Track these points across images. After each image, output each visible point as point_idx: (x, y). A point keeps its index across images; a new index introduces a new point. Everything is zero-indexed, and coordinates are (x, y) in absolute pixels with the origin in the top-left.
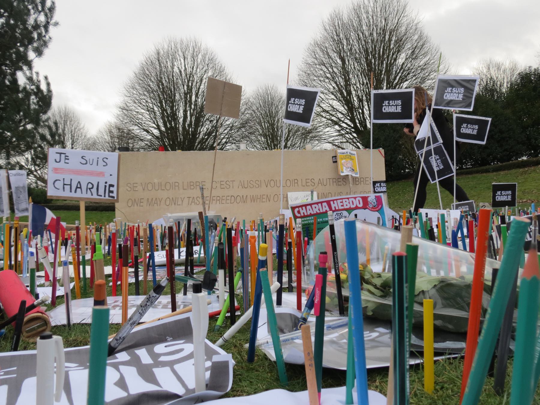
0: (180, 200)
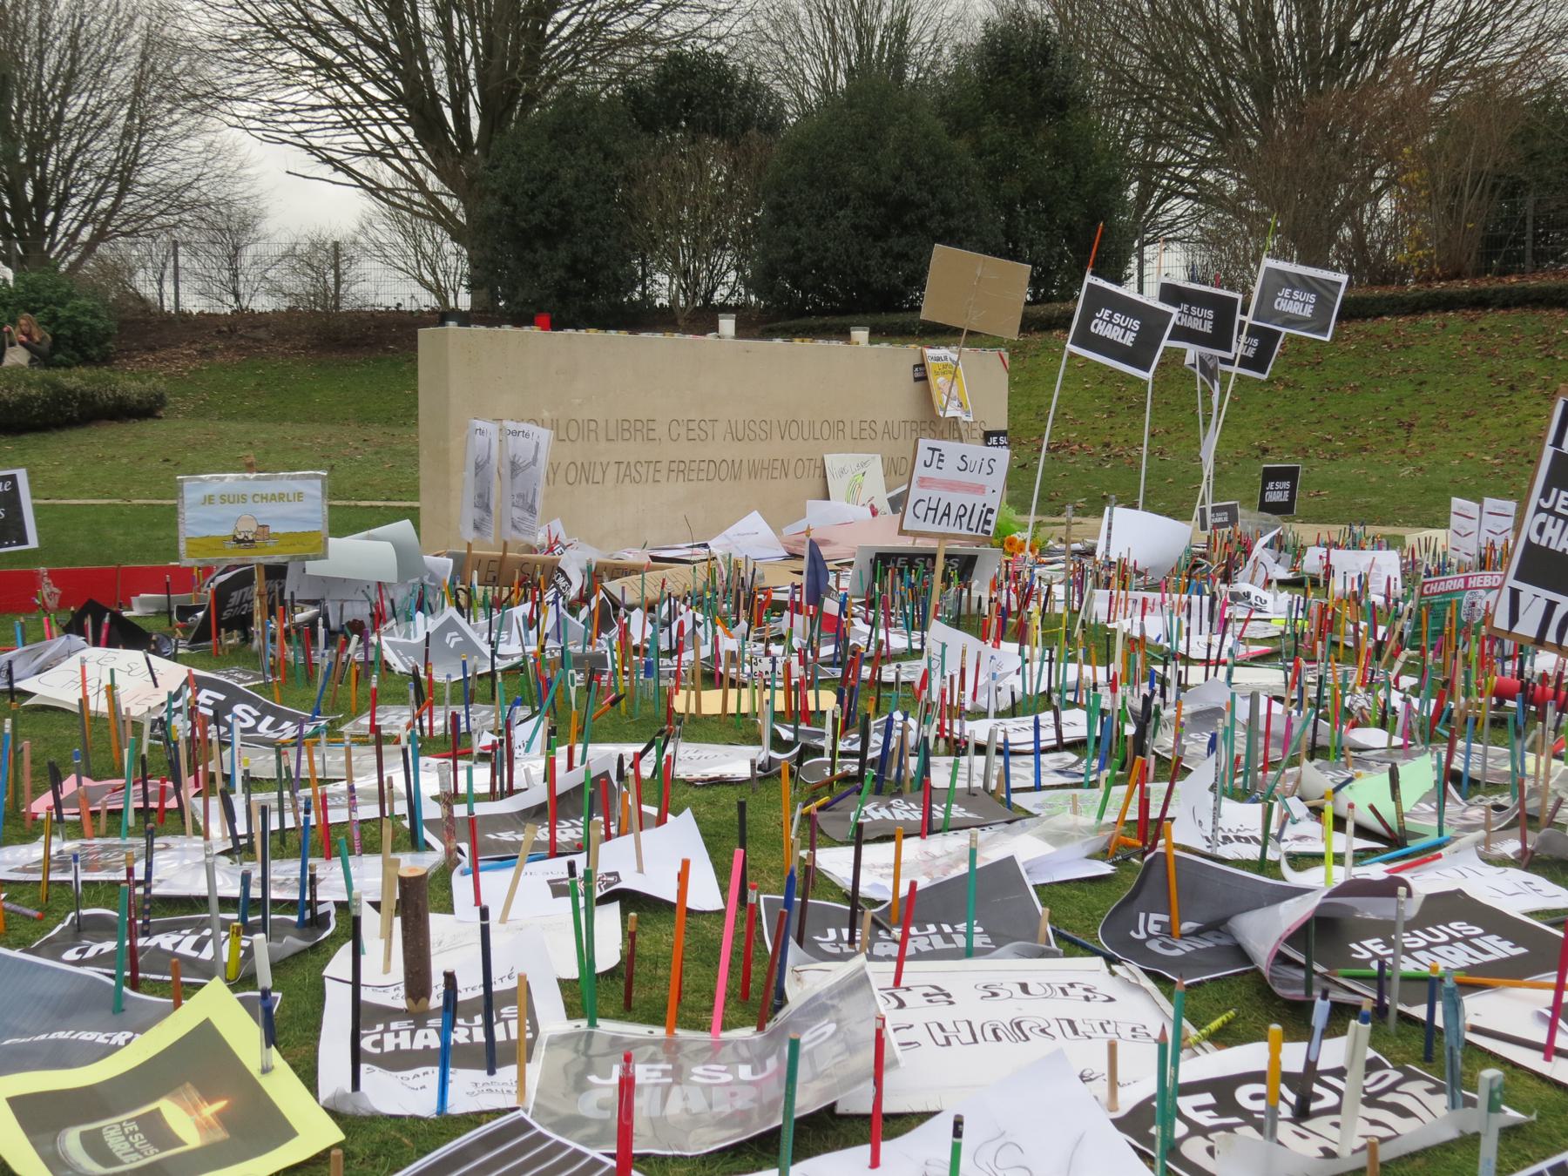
0: (598, 467)
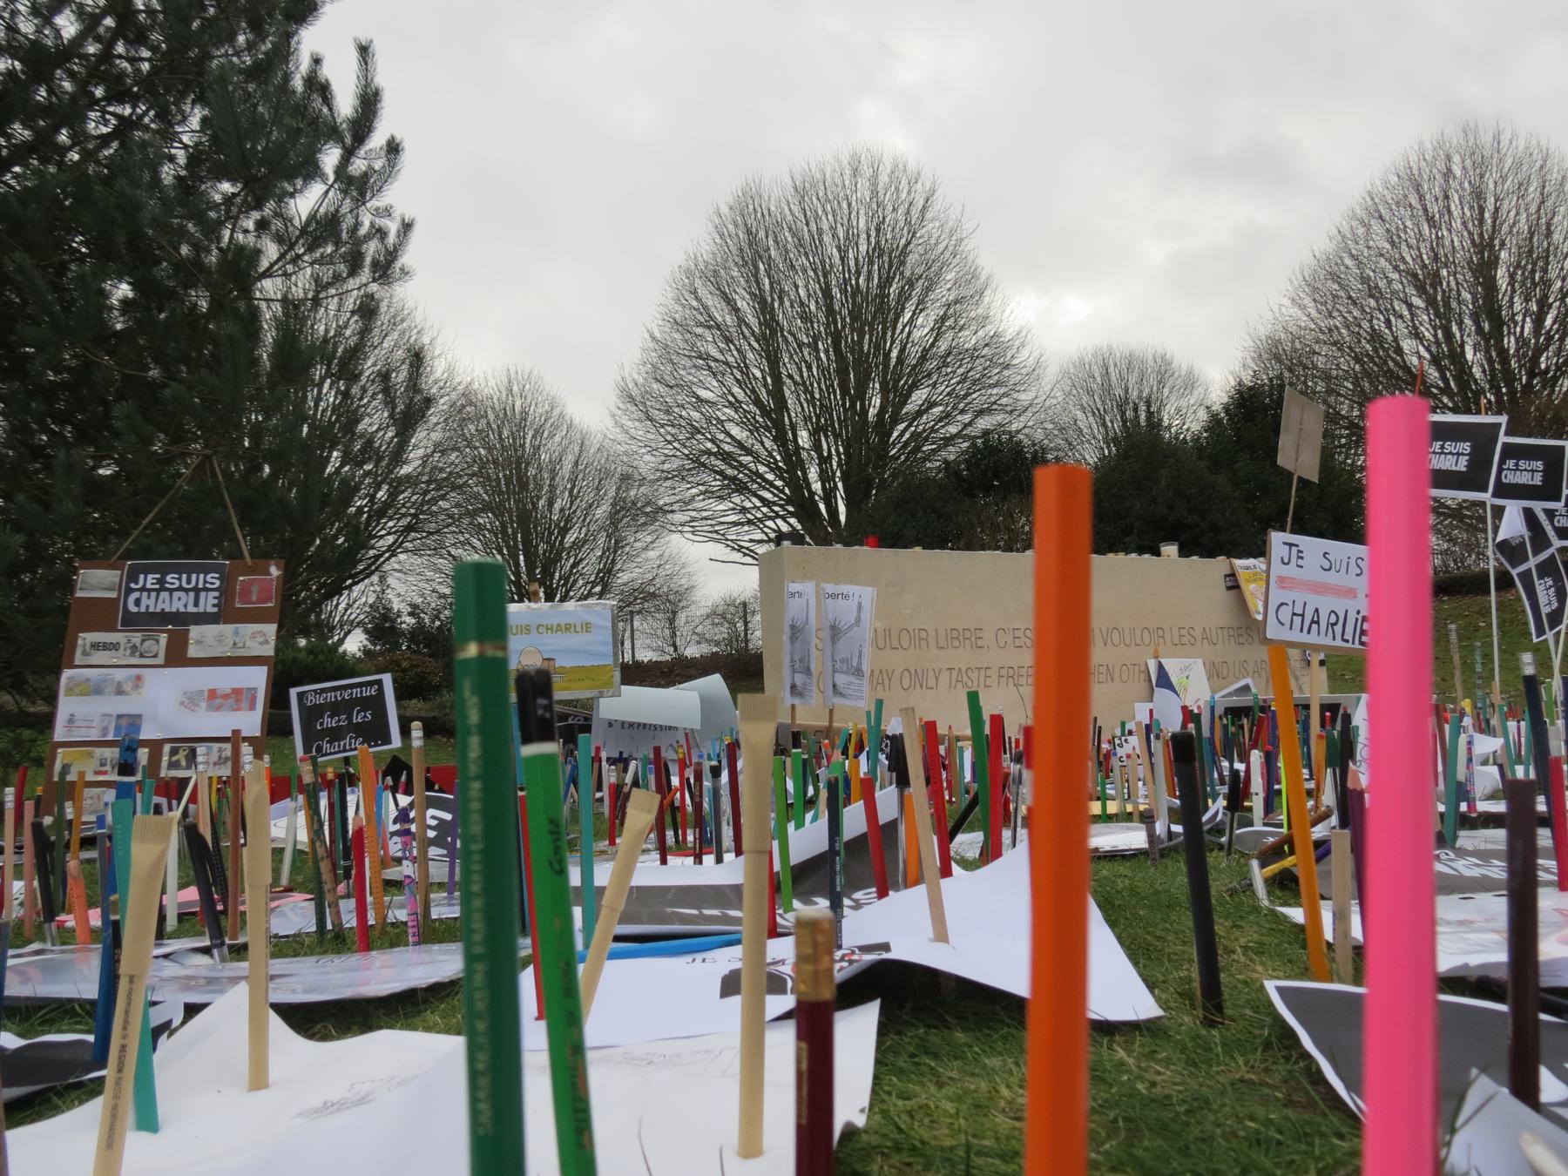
0: (931, 674)
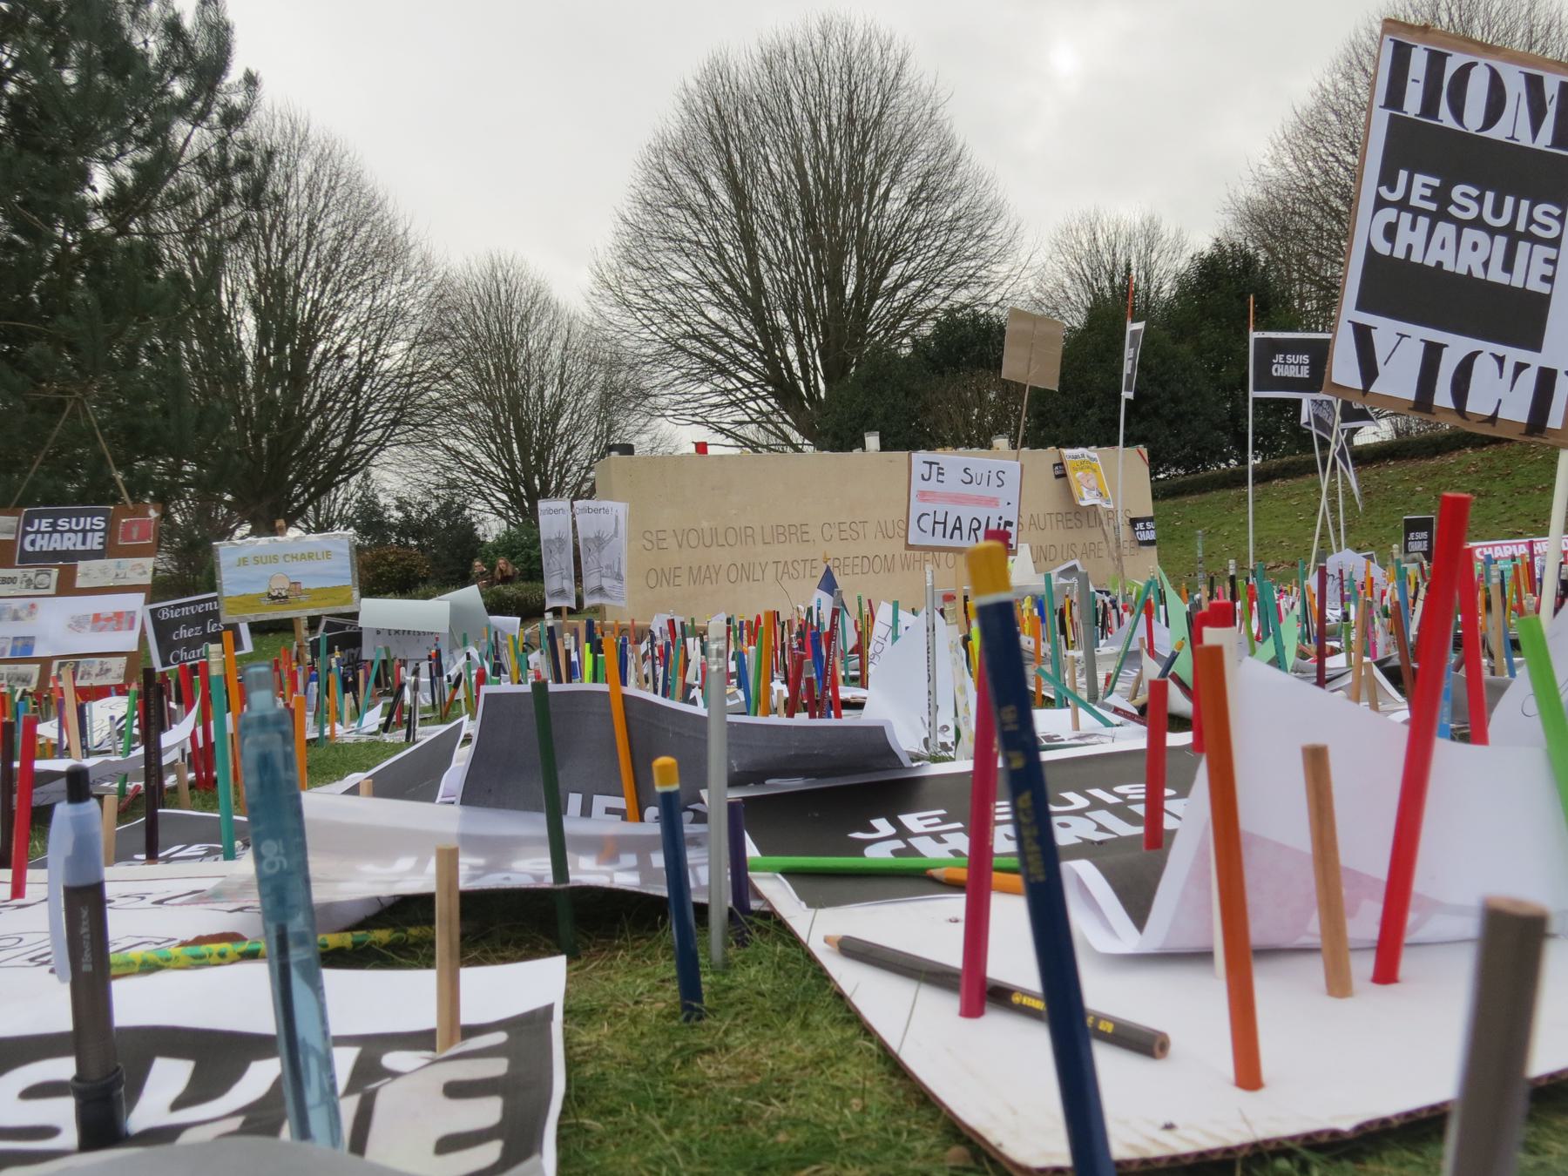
0: (758, 568)
